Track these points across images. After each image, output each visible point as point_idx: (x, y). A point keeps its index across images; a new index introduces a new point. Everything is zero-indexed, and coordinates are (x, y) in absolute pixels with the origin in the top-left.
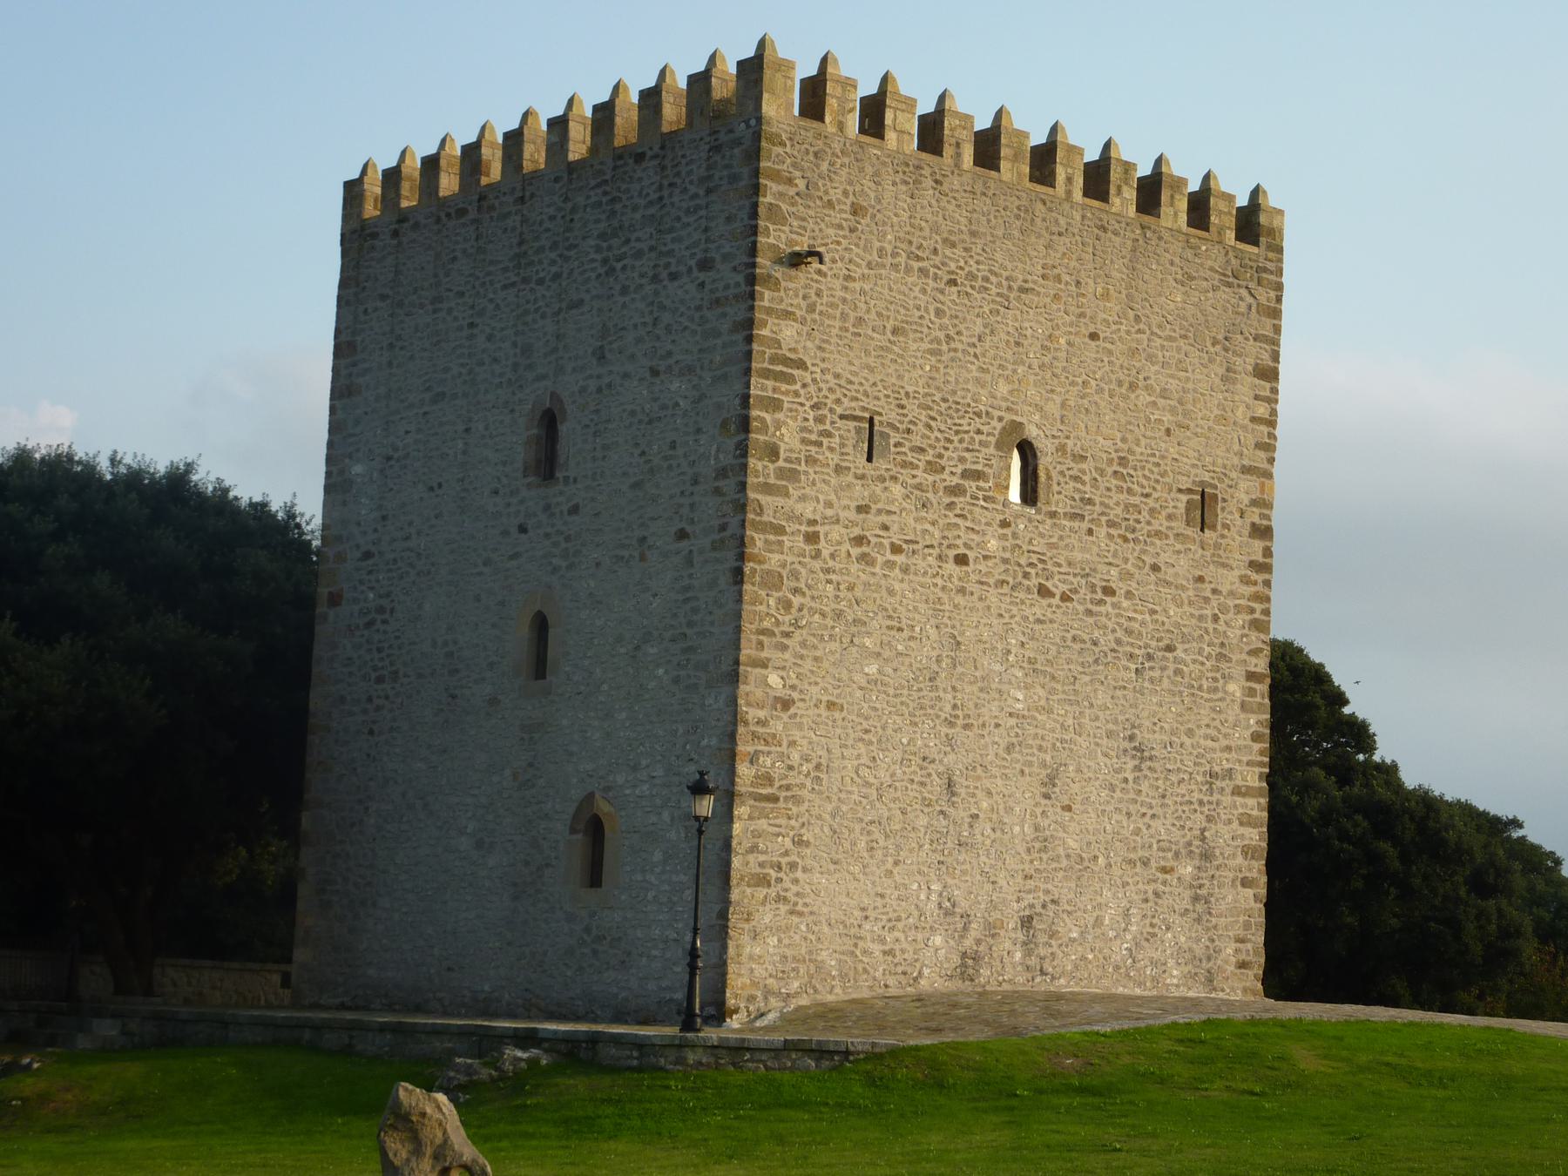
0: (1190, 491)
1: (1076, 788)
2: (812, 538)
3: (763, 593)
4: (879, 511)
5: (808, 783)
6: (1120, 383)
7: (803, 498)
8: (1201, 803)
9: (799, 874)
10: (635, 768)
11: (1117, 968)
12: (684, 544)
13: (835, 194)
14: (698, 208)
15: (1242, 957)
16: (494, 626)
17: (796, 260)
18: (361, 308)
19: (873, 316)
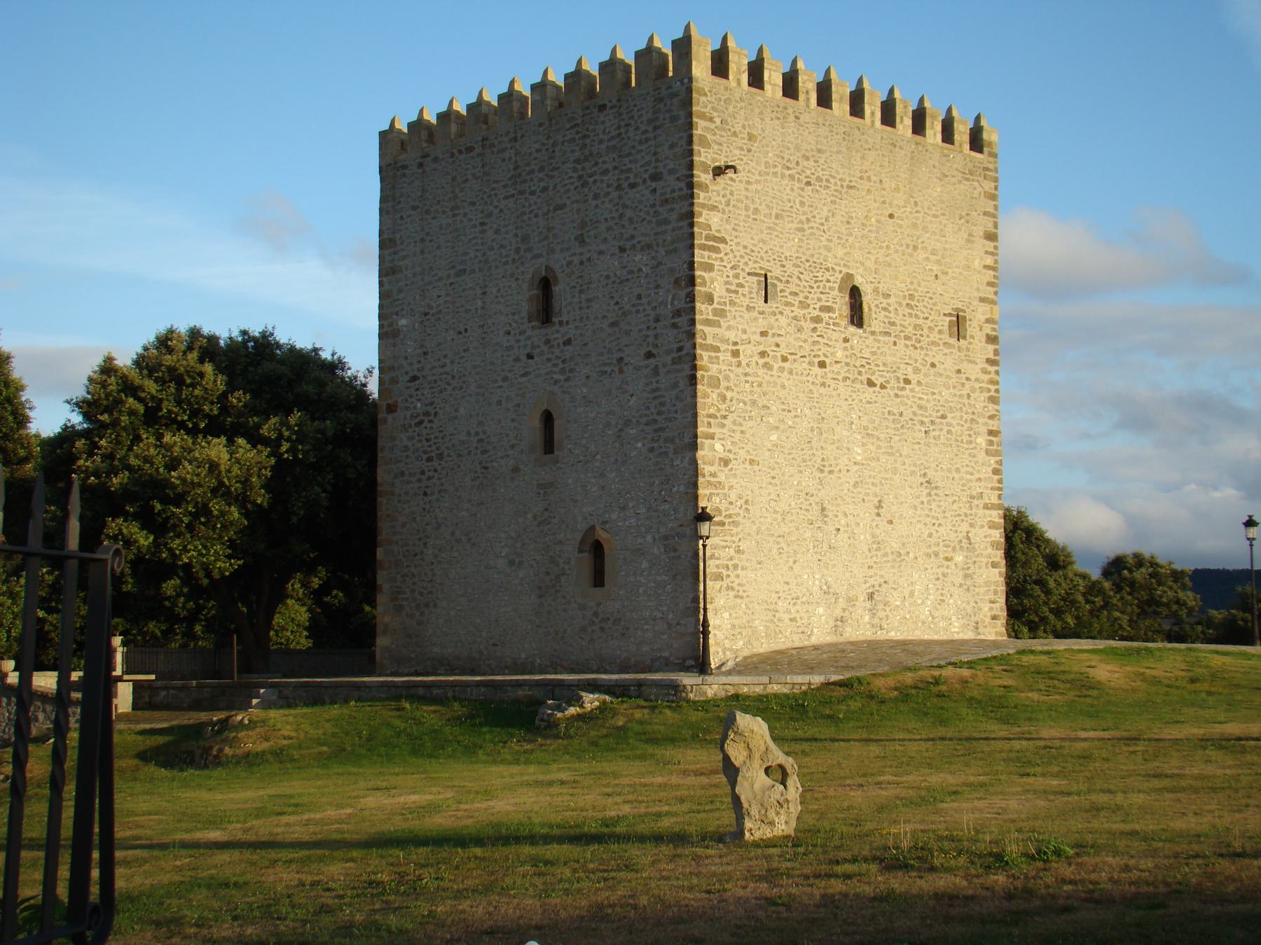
0: (950, 315)
1: (894, 508)
2: (736, 354)
3: (709, 390)
4: (774, 335)
5: (741, 512)
6: (908, 246)
7: (729, 328)
8: (966, 515)
9: (739, 571)
10: (624, 508)
11: (924, 623)
12: (652, 361)
13: (738, 128)
14: (647, 140)
15: (994, 612)
16: (513, 420)
17: (718, 172)
18: (398, 216)
19: (764, 206)
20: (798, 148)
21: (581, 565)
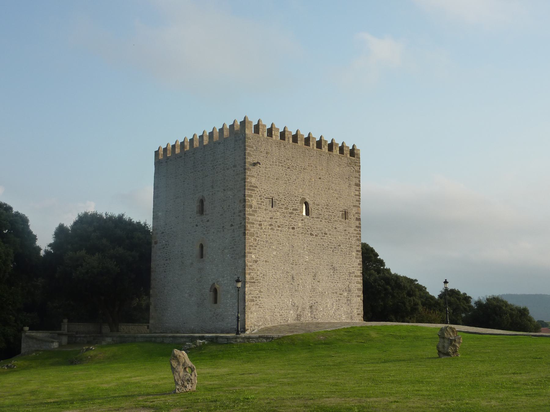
1: (320, 277)
2: (260, 225)
7: (258, 216)
9: (261, 299)
12: (233, 227)
13: (262, 150)
17: (254, 164)
20: (285, 156)
21: (209, 296)
